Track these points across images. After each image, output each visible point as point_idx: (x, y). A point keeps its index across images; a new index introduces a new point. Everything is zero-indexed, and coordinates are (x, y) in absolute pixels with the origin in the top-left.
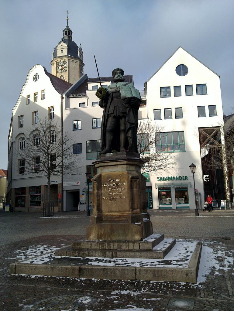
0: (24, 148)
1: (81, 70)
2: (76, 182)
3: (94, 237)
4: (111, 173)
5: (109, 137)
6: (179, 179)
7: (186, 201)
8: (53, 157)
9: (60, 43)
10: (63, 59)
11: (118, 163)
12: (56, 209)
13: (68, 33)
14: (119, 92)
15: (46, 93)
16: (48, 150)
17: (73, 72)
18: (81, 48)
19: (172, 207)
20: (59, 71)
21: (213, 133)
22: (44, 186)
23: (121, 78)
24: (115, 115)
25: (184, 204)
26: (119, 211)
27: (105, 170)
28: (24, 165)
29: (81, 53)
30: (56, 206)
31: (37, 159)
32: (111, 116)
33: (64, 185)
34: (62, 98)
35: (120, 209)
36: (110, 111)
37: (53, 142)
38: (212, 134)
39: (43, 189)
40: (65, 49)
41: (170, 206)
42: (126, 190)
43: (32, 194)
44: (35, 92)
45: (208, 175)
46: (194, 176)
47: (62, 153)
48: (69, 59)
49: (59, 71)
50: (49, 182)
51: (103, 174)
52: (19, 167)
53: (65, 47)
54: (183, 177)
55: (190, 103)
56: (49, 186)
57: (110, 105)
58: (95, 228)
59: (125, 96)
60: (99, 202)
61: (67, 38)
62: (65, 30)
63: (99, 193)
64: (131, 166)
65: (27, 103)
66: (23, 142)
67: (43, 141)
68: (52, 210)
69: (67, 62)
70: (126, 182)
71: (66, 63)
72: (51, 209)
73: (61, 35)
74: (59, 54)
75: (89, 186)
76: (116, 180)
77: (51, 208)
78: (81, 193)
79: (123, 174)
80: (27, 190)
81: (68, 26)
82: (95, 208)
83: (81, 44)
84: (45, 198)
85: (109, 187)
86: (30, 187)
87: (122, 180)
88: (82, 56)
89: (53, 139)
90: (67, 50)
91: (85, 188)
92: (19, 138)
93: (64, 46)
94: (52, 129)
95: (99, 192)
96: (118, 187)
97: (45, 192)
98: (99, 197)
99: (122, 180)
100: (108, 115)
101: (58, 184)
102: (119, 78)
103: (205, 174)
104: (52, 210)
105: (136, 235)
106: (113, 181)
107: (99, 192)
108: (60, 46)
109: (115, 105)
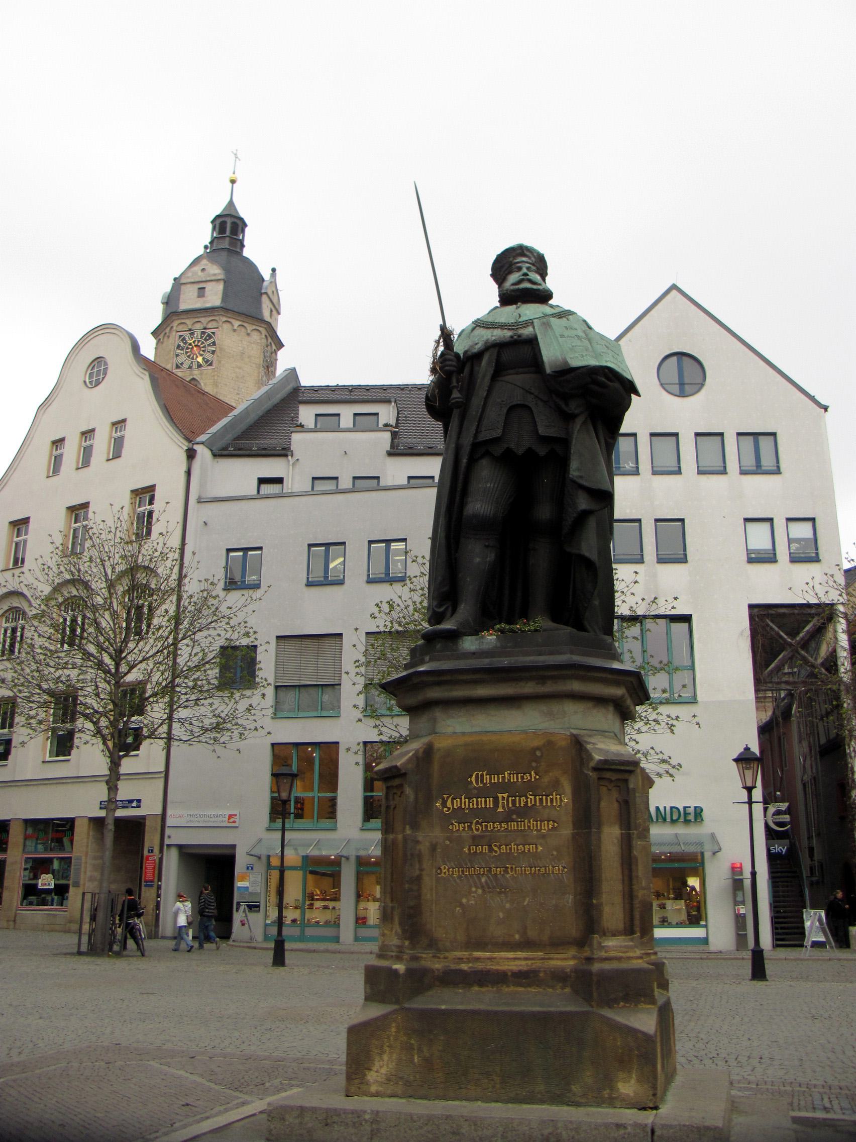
3: (389, 1080)
5: (478, 556)
6: (668, 819)
7: (696, 917)
11: (529, 688)
14: (532, 342)
15: (129, 433)
17: (237, 370)
19: (705, 941)
20: (182, 364)
21: (806, 629)
22: (86, 821)
23: (535, 287)
26: (527, 944)
27: (449, 722)
29: (275, 301)
33: (169, 822)
34: (191, 455)
35: (532, 934)
38: (801, 635)
39: (81, 832)
40: (213, 283)
42: (567, 831)
43: (36, 851)
44: (84, 429)
45: (787, 804)
49: (182, 364)
50: (110, 804)
53: (215, 275)
54: (685, 808)
57: (487, 398)
58: (393, 1030)
61: (226, 244)
62: (218, 217)
63: (418, 842)
65: (48, 472)
70: (567, 787)
73: (205, 234)
75: (286, 833)
76: (513, 779)
78: (241, 862)
79: (550, 743)
80: (16, 835)
81: (231, 204)
82: (392, 919)
83: (274, 270)
84: (88, 874)
86: (27, 822)
87: (546, 779)
88: (275, 312)
89: (138, 621)
90: (220, 287)
96: (524, 812)
97: (87, 846)
98: (420, 862)
99: (546, 779)
100: (475, 446)
101: (144, 818)
102: (527, 285)
103: (776, 800)
105: (621, 1075)
106: (495, 779)
107: (420, 839)
109: (515, 403)
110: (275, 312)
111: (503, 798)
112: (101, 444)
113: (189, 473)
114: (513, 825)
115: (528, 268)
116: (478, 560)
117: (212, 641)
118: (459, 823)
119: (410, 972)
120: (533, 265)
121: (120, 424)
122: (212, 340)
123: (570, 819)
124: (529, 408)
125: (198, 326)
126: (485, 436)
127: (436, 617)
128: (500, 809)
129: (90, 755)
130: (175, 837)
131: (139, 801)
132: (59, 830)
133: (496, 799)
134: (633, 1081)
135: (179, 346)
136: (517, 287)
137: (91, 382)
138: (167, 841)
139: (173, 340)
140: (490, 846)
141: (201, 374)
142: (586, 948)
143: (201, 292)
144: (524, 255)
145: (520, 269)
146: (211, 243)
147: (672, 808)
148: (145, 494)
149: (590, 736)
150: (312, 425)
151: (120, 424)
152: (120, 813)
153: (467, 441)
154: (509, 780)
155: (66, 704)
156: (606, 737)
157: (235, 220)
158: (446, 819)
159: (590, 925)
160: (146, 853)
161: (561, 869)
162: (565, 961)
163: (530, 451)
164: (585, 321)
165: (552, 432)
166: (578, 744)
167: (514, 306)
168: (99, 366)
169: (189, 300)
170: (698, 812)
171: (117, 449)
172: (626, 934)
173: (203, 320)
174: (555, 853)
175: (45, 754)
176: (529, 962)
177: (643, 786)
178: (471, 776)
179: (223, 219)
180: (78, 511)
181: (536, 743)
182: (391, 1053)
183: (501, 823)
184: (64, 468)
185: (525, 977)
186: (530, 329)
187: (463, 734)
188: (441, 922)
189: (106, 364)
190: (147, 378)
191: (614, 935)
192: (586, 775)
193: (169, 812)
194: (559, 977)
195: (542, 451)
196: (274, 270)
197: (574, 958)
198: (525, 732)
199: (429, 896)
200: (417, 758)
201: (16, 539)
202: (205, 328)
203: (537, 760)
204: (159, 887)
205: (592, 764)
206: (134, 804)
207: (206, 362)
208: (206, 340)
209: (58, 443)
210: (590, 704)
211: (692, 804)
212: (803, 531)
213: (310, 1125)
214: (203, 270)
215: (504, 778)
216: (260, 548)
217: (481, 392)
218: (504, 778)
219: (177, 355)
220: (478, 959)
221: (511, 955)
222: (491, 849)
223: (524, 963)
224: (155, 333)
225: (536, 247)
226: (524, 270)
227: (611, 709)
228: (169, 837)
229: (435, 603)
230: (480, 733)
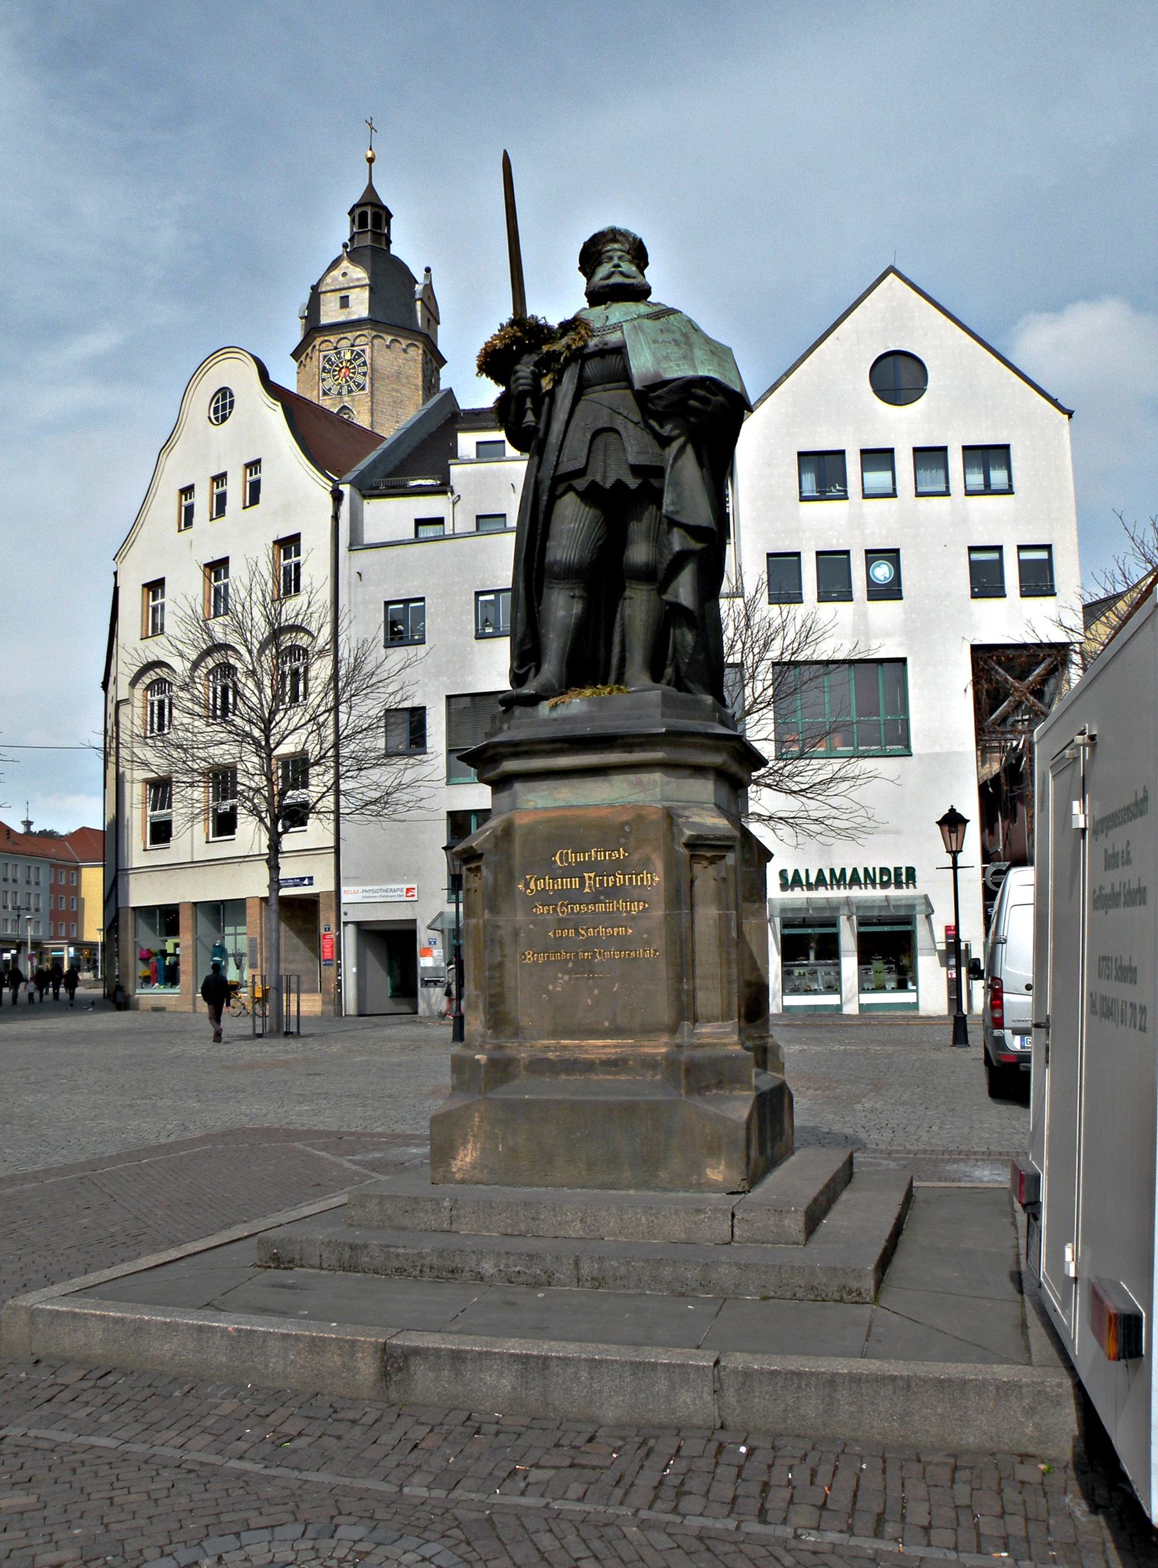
0: (166, 731)
1: (430, 383)
2: (400, 886)
4: (569, 813)
5: (562, 608)
8: (298, 768)
9: (336, 263)
10: (349, 335)
12: (311, 1004)
13: (372, 218)
15: (265, 476)
16: (267, 732)
18: (429, 287)
19: (915, 1006)
20: (330, 390)
22: (258, 901)
24: (598, 478)
25: (893, 990)
26: (617, 1031)
27: (530, 796)
28: (170, 807)
29: (432, 309)
30: (314, 991)
31: (222, 779)
32: (571, 488)
33: (344, 898)
34: (337, 496)
36: (564, 458)
37: (295, 698)
41: (832, 1000)
42: (659, 912)
44: (215, 473)
46: (955, 867)
47: (336, 746)
48: (375, 333)
49: (330, 390)
50: (276, 883)
51: (521, 820)
52: (149, 813)
53: (358, 279)
55: (939, 530)
56: (273, 901)
57: (568, 423)
59: (658, 374)
60: (501, 977)
61: (367, 240)
62: (356, 206)
63: (499, 927)
64: (691, 776)
66: (161, 703)
67: (247, 693)
68: (294, 1008)
69: (367, 348)
70: (659, 865)
71: (363, 351)
72: (288, 1006)
73: (343, 230)
74: (331, 313)
77: (288, 1000)
78: (423, 936)
81: (370, 189)
83: (428, 270)
85: (563, 894)
87: (636, 857)
88: (432, 322)
89: (290, 687)
90: (366, 294)
91: (441, 914)
92: (147, 679)
93: (355, 276)
94: (287, 641)
95: (501, 920)
96: (613, 893)
99: (636, 857)
100: (557, 480)
101: (317, 895)
102: (617, 279)
104: (294, 1008)
106: (580, 858)
107: (501, 923)
108: (335, 279)
109: (600, 426)
110: (432, 322)
111: (590, 878)
112: (235, 490)
113: (336, 518)
114: (601, 907)
115: (620, 258)
116: (561, 613)
117: (370, 708)
118: (544, 906)
119: (492, 1062)
120: (628, 253)
121: (254, 466)
122: (362, 360)
123: (662, 899)
124: (617, 432)
125: (344, 343)
126: (566, 467)
127: (517, 679)
128: (587, 890)
129: (250, 834)
130: (352, 914)
131: (311, 878)
132: (222, 912)
133: (582, 879)
134: (722, 1168)
135: (324, 368)
136: (606, 282)
137: (217, 419)
138: (343, 919)
139: (316, 361)
140: (576, 930)
141: (353, 401)
142: (678, 1035)
143: (345, 302)
144: (615, 241)
145: (611, 259)
146: (351, 239)
147: (881, 869)
148: (289, 544)
149: (684, 808)
150: (473, 456)
151: (254, 466)
152: (284, 892)
153: (547, 473)
154: (596, 858)
155: (222, 779)
156: (703, 808)
157: (377, 210)
158: (530, 902)
159: (686, 1011)
160: (322, 931)
161: (654, 953)
162: (658, 1047)
163: (619, 483)
164: (690, 321)
165: (643, 460)
166: (670, 816)
167: (603, 307)
168: (224, 398)
169: (331, 313)
170: (911, 872)
171: (254, 493)
172: (723, 1020)
173: (332, 338)
174: (645, 936)
175: (207, 834)
176: (619, 1050)
177: (759, 859)
178: (555, 855)
179: (363, 209)
180: (218, 567)
181: (625, 818)
182: (475, 1143)
183: (587, 905)
184: (196, 520)
185: (614, 1065)
186: (618, 334)
187: (546, 809)
188: (525, 1008)
189: (231, 395)
190: (279, 409)
191: (709, 1021)
192: (677, 851)
193: (343, 889)
194: (650, 1064)
195: (633, 483)
196: (428, 270)
197: (666, 1044)
198: (611, 806)
199: (513, 983)
200: (496, 837)
201: (151, 603)
202: (353, 346)
203: (626, 836)
204: (339, 966)
205: (683, 840)
206: (306, 882)
207: (358, 386)
208: (355, 359)
209: (187, 491)
210: (687, 772)
211: (904, 864)
212: (882, 572)
213: (389, 1212)
214: (344, 274)
215: (590, 856)
216: (422, 599)
217: (561, 414)
218: (590, 856)
219: (324, 380)
220: (565, 1047)
221: (600, 1042)
222: (577, 933)
223: (613, 1051)
224: (296, 355)
225: (631, 230)
226: (616, 261)
227: (712, 777)
228: (346, 914)
229: (515, 665)
230: (563, 807)
